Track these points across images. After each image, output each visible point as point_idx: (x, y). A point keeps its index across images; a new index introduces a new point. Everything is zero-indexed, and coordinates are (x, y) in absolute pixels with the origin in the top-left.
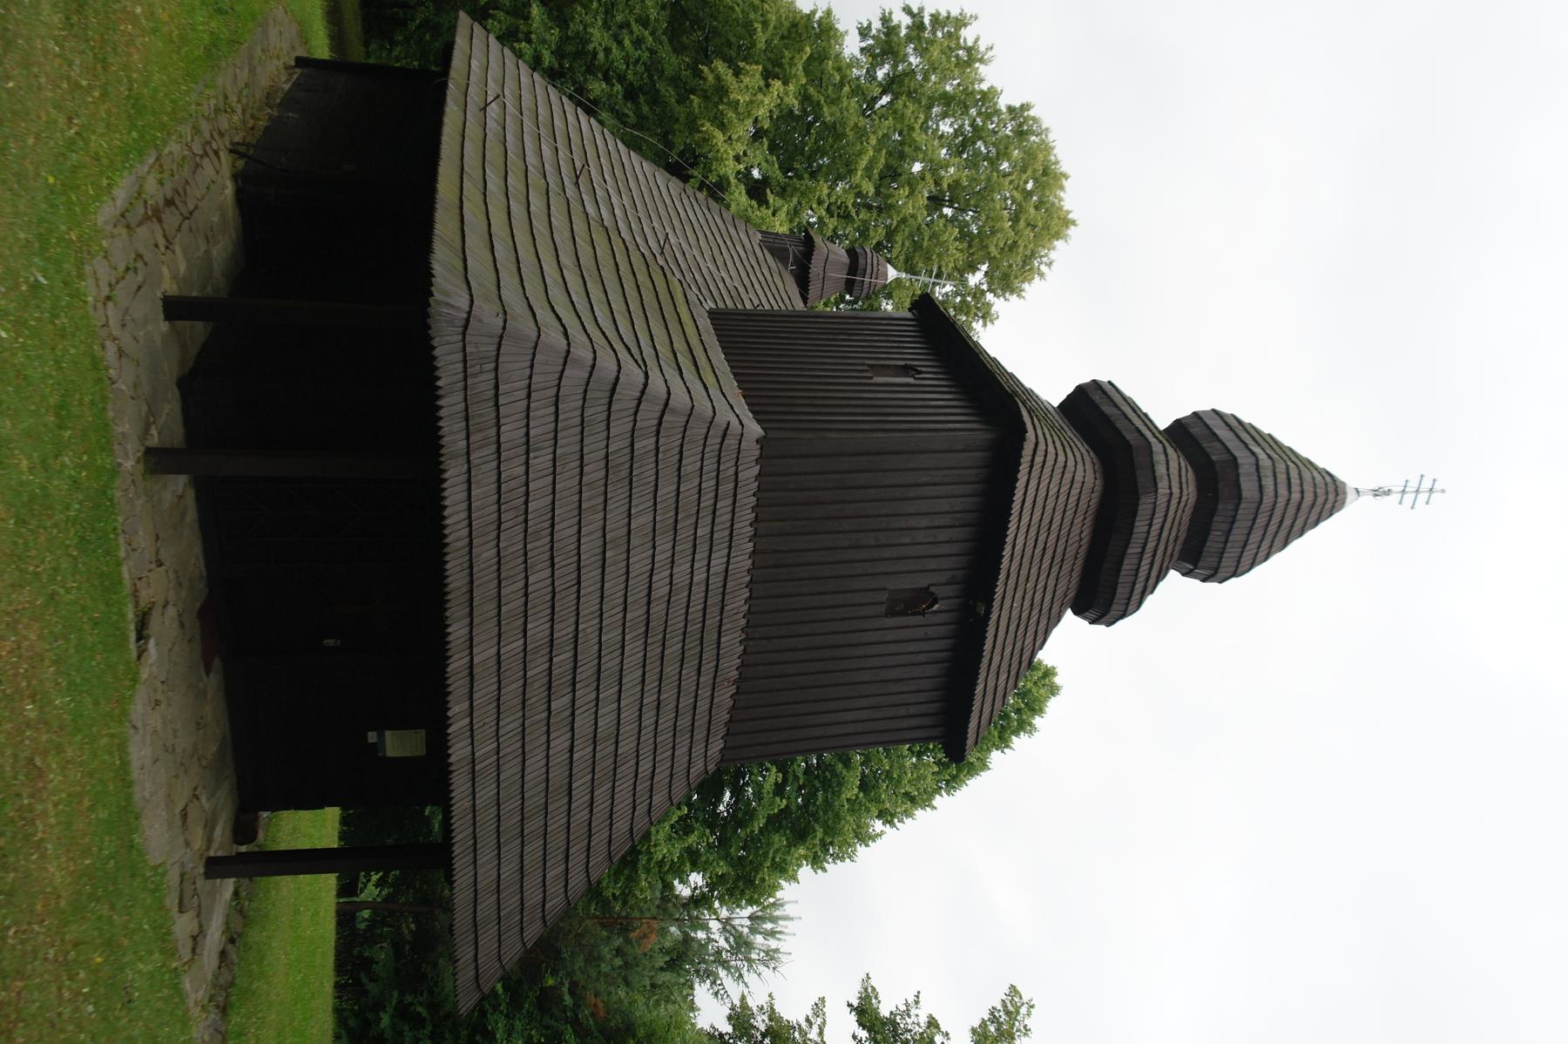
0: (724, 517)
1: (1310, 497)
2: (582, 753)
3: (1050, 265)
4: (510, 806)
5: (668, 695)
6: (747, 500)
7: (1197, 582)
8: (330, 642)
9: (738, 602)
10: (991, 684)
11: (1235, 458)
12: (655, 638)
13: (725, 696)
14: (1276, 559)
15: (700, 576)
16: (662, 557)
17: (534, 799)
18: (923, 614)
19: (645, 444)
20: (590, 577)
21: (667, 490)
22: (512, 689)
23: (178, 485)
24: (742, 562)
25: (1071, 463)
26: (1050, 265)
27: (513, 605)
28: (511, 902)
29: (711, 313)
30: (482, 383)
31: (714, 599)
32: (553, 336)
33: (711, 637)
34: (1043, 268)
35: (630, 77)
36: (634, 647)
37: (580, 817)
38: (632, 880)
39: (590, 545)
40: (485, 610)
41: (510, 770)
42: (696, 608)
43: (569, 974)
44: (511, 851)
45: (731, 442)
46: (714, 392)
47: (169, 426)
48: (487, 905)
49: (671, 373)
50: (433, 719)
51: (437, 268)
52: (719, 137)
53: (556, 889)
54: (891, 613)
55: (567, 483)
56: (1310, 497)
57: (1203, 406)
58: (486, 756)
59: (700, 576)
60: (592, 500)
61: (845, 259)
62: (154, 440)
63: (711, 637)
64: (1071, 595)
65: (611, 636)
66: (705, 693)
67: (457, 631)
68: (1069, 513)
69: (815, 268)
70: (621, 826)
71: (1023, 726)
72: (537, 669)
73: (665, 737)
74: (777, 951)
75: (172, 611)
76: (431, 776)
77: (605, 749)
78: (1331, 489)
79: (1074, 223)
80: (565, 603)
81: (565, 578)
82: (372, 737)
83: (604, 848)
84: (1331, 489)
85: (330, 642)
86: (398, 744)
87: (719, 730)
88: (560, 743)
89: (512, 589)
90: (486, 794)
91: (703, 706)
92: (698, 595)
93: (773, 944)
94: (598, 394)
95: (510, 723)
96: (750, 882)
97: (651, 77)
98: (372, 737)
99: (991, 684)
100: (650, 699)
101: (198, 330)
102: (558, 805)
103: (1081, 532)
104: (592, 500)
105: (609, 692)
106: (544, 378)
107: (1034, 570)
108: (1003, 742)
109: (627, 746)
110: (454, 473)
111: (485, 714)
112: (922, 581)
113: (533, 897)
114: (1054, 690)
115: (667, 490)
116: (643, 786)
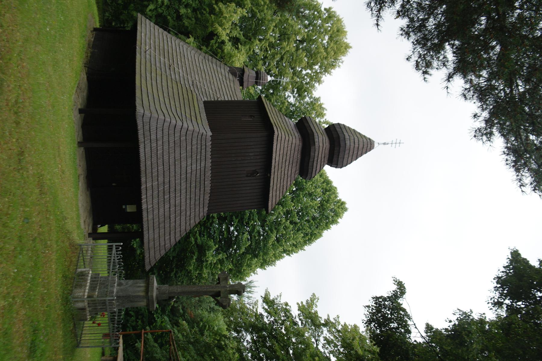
0: (203, 154)
1: (366, 145)
2: (172, 209)
3: (342, 62)
4: (156, 220)
5: (193, 196)
6: (209, 150)
7: (339, 169)
8: (114, 184)
9: (209, 174)
10: (274, 194)
11: (339, 136)
12: (189, 182)
13: (207, 197)
14: (354, 162)
15: (198, 168)
16: (189, 163)
17: (162, 219)
18: (255, 176)
19: (183, 138)
20: (172, 168)
21: (189, 148)
22: (155, 193)
23: (82, 149)
24: (209, 164)
25: (291, 139)
26: (342, 62)
27: (155, 174)
28: (157, 244)
29: (205, 102)
30: (147, 127)
31: (202, 173)
32: (161, 117)
33: (202, 182)
34: (340, 64)
35: (194, 5)
36: (183, 184)
37: (173, 225)
38: (201, 270)
39: (172, 161)
40: (149, 175)
41: (156, 212)
42: (198, 175)
43: (182, 303)
44: (157, 231)
45: (204, 137)
46: (200, 125)
47: (80, 139)
48: (151, 244)
49: (189, 122)
50: (138, 201)
51: (137, 105)
52: (220, 29)
53: (167, 242)
54: (247, 176)
55: (166, 147)
56: (366, 145)
57: (342, 122)
58: (150, 208)
59: (198, 168)
60: (172, 151)
61: (255, 75)
62: (79, 141)
63: (202, 182)
64: (298, 172)
65: (178, 181)
66: (202, 196)
67: (143, 180)
68: (292, 151)
69: (245, 78)
70: (183, 228)
71: (334, 222)
72: (161, 189)
73: (192, 206)
74: (251, 297)
75: (82, 176)
76: (138, 217)
77: (178, 208)
78: (369, 143)
79: (351, 47)
80: (167, 173)
81: (166, 168)
82: (124, 207)
83: (179, 233)
84: (369, 143)
85: (114, 184)
86: (130, 209)
87: (206, 205)
88: (167, 206)
89: (155, 170)
90: (150, 217)
91: (202, 199)
92: (198, 172)
93: (250, 295)
94: (172, 128)
95: (155, 201)
96: (240, 272)
97: (201, 5)
98: (124, 207)
99: (274, 194)
100: (188, 197)
101: (83, 115)
102: (167, 221)
103: (297, 156)
104: (172, 151)
105: (178, 195)
106: (160, 125)
107: (283, 166)
108: (327, 227)
109: (183, 208)
110: (141, 146)
111: (150, 199)
112: (254, 169)
113: (162, 244)
114: (346, 210)
115: (189, 148)
116: (188, 218)
